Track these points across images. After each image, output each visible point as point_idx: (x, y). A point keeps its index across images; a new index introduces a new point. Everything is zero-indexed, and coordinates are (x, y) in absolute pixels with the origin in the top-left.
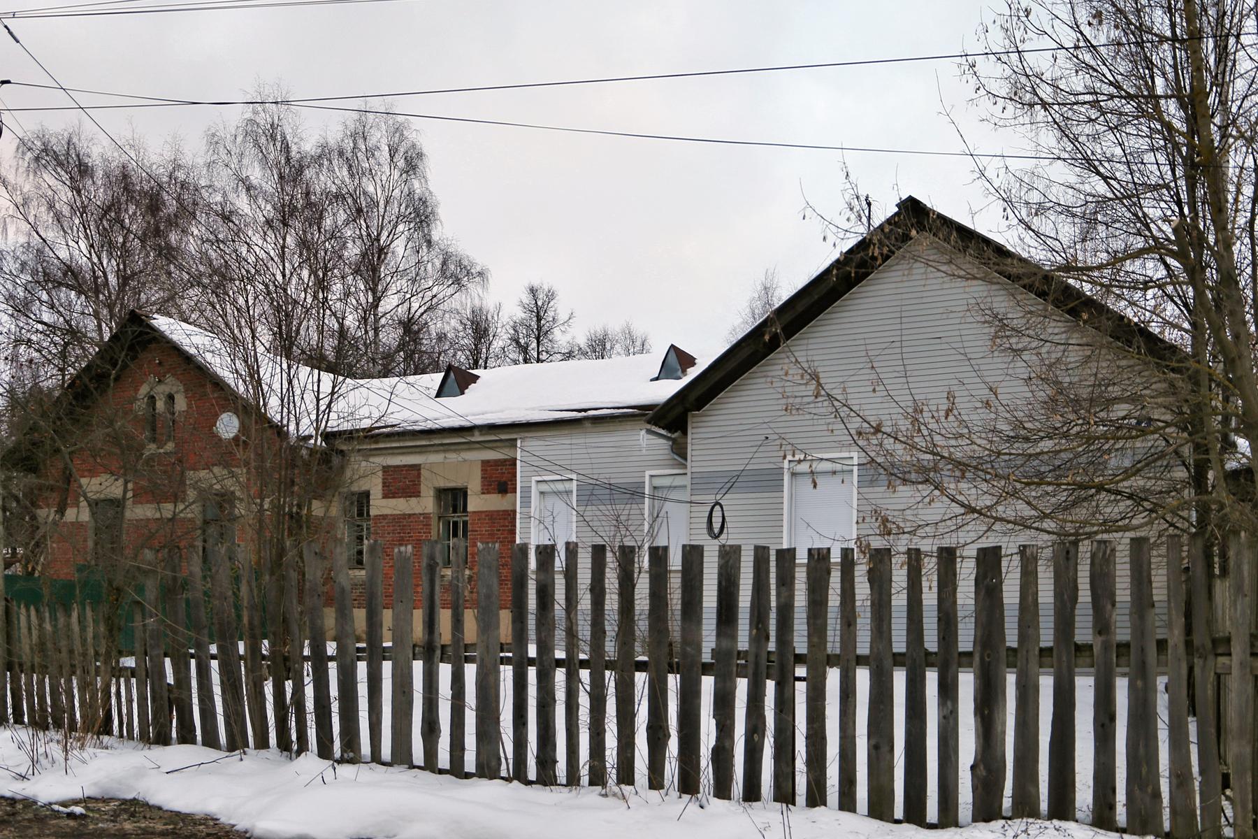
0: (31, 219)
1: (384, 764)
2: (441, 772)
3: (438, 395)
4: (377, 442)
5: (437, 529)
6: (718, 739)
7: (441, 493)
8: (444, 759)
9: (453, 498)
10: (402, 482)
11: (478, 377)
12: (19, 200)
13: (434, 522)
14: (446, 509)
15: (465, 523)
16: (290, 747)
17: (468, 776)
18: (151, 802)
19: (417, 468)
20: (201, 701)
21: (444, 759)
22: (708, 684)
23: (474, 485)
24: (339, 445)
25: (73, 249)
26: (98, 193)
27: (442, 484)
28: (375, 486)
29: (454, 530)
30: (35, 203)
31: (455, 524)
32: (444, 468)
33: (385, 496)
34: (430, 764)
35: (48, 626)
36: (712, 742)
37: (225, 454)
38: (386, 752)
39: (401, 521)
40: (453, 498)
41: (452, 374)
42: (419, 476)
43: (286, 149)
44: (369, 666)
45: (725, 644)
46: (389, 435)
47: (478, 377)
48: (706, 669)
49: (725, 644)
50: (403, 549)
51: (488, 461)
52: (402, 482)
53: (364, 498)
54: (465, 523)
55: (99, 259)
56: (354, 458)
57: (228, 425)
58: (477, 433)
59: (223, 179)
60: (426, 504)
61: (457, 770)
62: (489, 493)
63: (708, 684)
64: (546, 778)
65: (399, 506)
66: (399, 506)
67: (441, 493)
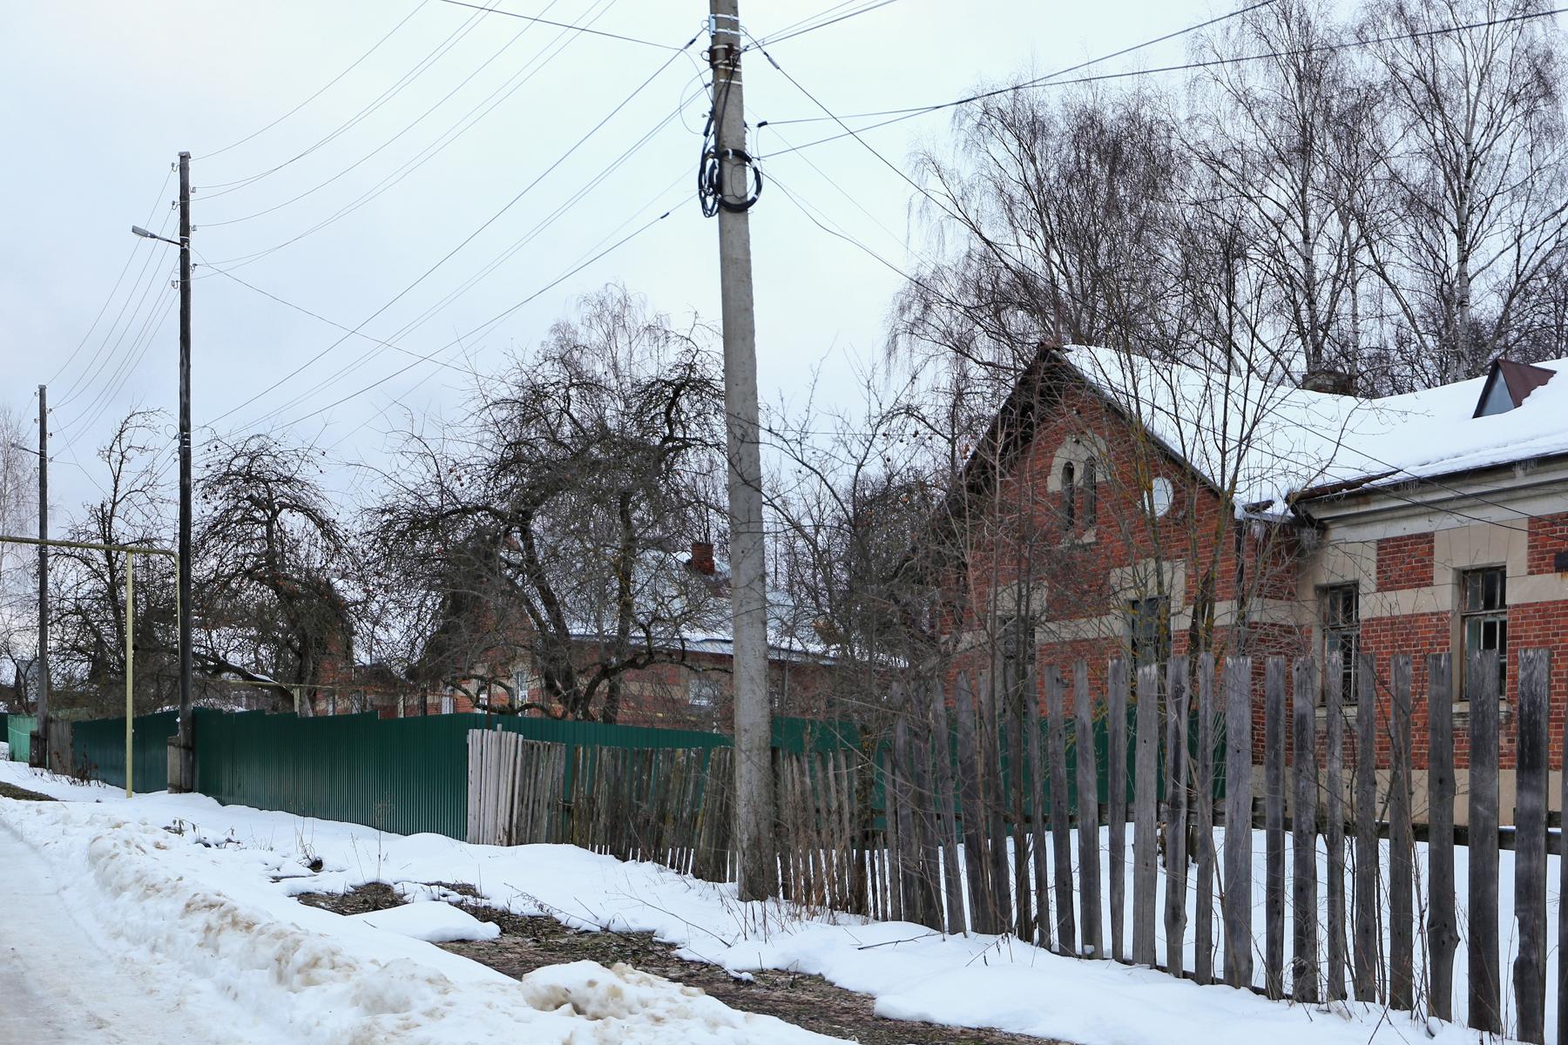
0: (972, 216)
1: (1125, 962)
2: (1186, 975)
3: (1478, 413)
4: (1368, 503)
5: (1457, 635)
6: (1523, 947)
7: (1465, 577)
8: (1189, 962)
9: (1485, 583)
10: (1406, 563)
11: (1552, 373)
12: (957, 192)
13: (1454, 626)
14: (1475, 604)
15: (1503, 624)
16: (711, 871)
17: (1214, 981)
18: (828, 978)
19: (1427, 538)
20: (946, 870)
21: (1189, 962)
22: (1507, 861)
23: (1515, 557)
24: (1318, 508)
25: (1026, 251)
26: (1057, 154)
27: (1464, 563)
28: (1365, 571)
29: (1492, 636)
30: (977, 193)
31: (1490, 628)
32: (1465, 539)
33: (1382, 587)
34: (1173, 967)
35: (808, 780)
36: (1515, 954)
37: (1163, 538)
38: (1128, 950)
39: (1400, 628)
40: (1485, 583)
41: (1501, 376)
42: (1431, 552)
43: (1306, 27)
44: (1112, 831)
45: (1531, 801)
46: (1396, 486)
47: (1552, 373)
48: (1504, 840)
49: (1531, 801)
50: (1147, 669)
51: (1540, 519)
52: (1406, 563)
53: (1347, 594)
54: (1503, 624)
55: (1503, 112)
56: (1337, 533)
57: (1161, 496)
58: (1519, 472)
59: (1216, 100)
60: (1441, 597)
61: (1202, 976)
62: (1540, 572)
63: (1507, 861)
64: (1305, 995)
65: (1406, 602)
66: (1406, 602)
67: (1465, 577)
